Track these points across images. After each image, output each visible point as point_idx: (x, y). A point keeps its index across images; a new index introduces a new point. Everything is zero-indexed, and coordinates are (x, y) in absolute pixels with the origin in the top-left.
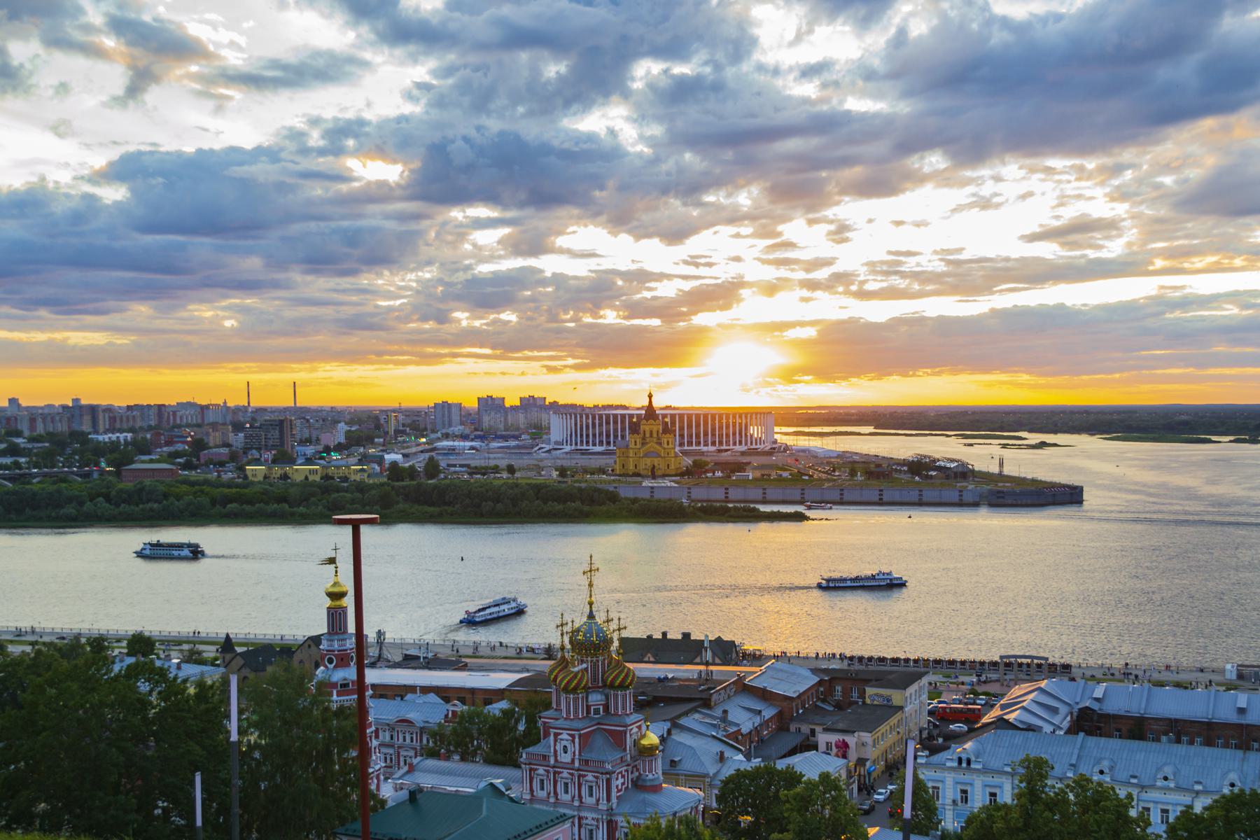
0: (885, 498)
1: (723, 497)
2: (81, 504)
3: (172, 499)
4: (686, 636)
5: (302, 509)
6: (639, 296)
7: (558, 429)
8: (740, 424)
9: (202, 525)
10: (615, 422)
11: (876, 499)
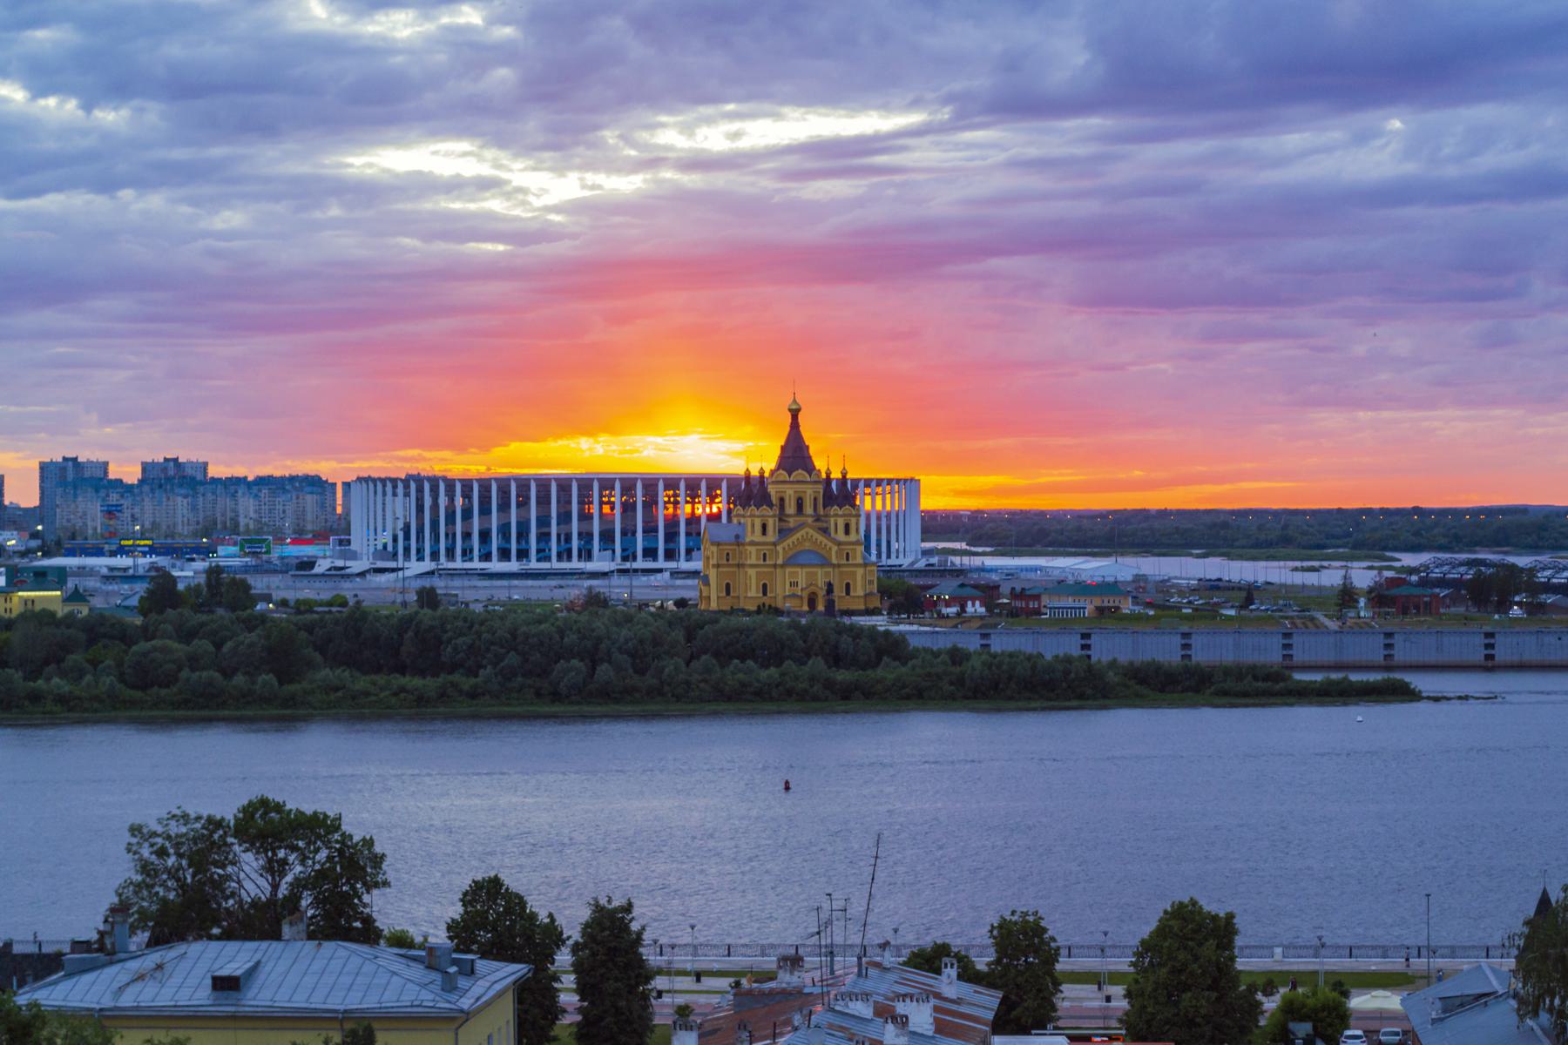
0: (1501, 655)
1: (1378, 657)
5: (59, 684)
6: (400, 206)
8: (672, 523)
10: (544, 500)
11: (1478, 657)
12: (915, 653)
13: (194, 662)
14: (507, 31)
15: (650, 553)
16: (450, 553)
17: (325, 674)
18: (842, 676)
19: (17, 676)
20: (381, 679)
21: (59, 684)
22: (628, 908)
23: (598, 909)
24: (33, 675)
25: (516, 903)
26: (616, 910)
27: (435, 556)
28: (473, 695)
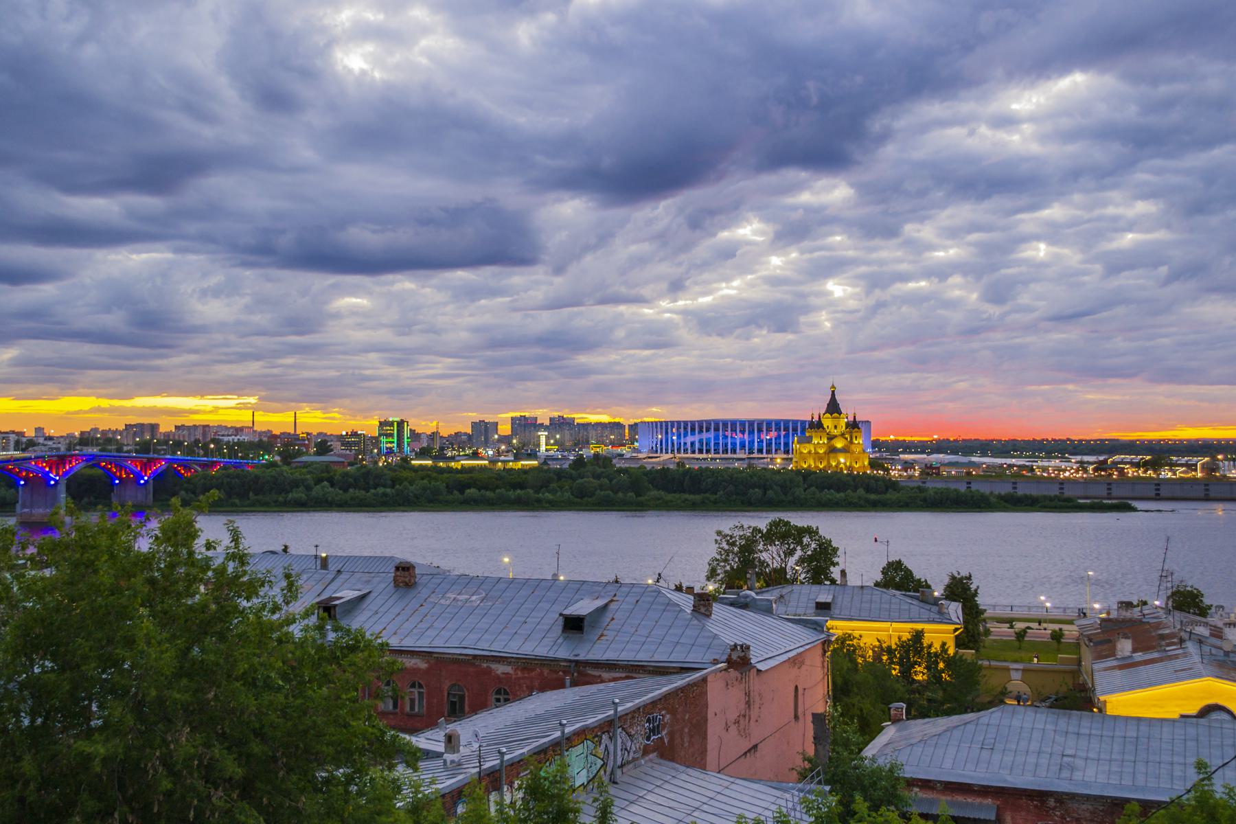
2: (308, 488)
3: (406, 483)
4: (976, 593)
5: (549, 496)
7: (337, 447)
9: (327, 511)
11: (1152, 494)
12: (903, 488)
13: (601, 487)
14: (759, 239)
15: (760, 451)
16: (679, 451)
17: (654, 493)
18: (873, 497)
19: (531, 491)
20: (677, 496)
21: (549, 496)
22: (969, 578)
23: (953, 578)
24: (537, 492)
25: (908, 573)
26: (962, 578)
27: (673, 451)
28: (715, 503)
